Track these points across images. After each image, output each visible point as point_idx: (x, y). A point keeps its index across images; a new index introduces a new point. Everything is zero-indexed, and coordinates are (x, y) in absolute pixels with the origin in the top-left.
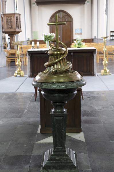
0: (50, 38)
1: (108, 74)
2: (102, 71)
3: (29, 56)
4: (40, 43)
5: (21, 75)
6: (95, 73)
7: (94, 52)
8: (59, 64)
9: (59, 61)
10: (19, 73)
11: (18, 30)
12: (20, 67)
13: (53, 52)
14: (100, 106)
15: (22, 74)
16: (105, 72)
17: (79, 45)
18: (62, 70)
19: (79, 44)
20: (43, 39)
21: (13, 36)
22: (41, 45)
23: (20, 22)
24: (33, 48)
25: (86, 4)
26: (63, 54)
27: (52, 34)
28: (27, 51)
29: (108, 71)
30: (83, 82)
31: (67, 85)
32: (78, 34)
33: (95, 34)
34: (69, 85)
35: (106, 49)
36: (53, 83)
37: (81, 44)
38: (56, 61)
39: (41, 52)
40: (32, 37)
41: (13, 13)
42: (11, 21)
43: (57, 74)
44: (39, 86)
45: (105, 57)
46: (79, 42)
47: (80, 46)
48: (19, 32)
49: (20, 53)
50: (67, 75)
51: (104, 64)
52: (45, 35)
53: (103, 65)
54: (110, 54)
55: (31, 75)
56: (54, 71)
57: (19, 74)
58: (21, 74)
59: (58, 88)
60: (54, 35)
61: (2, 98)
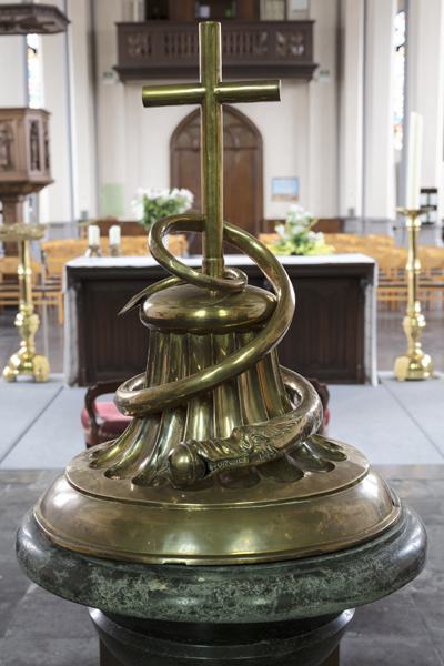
0: (171, 211)
1: (426, 375)
2: (402, 363)
3: (75, 288)
4: (123, 234)
5: (34, 377)
6: (367, 373)
7: (365, 277)
8: (222, 398)
9: (229, 382)
10: (27, 365)
11: (35, 176)
12: (31, 338)
13: (179, 311)
15: (40, 370)
16: (413, 366)
17: (298, 246)
18: (251, 455)
19: (297, 241)
20: (138, 213)
21: (17, 201)
22: (126, 239)
23: (46, 143)
24: (91, 255)
25: (316, 80)
26: (257, 326)
27: (178, 195)
28: (64, 275)
29: (426, 361)
30: (401, 547)
31: (293, 588)
32: (283, 197)
33: (352, 202)
34: (312, 583)
35: (418, 266)
36: (178, 574)
37: (306, 242)
38: (208, 376)
39: (129, 273)
40: (98, 207)
41: (20, 104)
42: (10, 136)
43: (211, 483)
44: (66, 584)
45: (415, 300)
46: (296, 230)
47: (301, 249)
48: (38, 186)
49: (32, 275)
50: (288, 491)
51: (408, 330)
52: (146, 198)
53: (403, 333)
54: (424, 284)
55: (80, 373)
56: (190, 467)
57: (28, 368)
58: (36, 369)
59: (220, 620)
60: (186, 196)
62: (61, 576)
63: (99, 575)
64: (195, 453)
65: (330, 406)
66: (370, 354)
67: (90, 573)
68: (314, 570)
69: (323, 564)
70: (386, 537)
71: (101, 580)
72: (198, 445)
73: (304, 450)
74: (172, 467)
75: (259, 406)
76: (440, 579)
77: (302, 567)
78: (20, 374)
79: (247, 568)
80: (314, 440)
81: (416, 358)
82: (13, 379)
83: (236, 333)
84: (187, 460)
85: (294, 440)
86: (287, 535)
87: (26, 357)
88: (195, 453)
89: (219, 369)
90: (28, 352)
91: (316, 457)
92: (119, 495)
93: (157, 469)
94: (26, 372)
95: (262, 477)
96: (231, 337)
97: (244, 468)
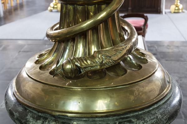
1: (180, 11)
2: (173, 7)
6: (161, 10)
9: (95, 28)
10: (55, 6)
14: (175, 73)
16: (177, 8)
29: (181, 6)
44: (17, 119)
57: (56, 8)
61: (22, 50)
62: (16, 114)
63: (31, 117)
64: (74, 64)
65: (149, 22)
66: (163, 4)
67: (27, 115)
68: (128, 119)
69: (133, 117)
70: (166, 99)
71: (31, 119)
72: (76, 60)
73: (128, 59)
74: (63, 69)
75: (108, 38)
76: (181, 80)
77: (123, 118)
78: (53, 9)
79: (96, 119)
80: (135, 53)
81: (178, 6)
82: (51, 11)
83: (98, 5)
84: (70, 67)
85: (125, 54)
86: (116, 103)
87: (55, 4)
88: (74, 64)
89: (92, 20)
90: (56, 2)
91: (134, 62)
92: (42, 80)
93: (57, 70)
94: (55, 9)
95: (107, 72)
96: (95, 7)
97: (98, 70)
